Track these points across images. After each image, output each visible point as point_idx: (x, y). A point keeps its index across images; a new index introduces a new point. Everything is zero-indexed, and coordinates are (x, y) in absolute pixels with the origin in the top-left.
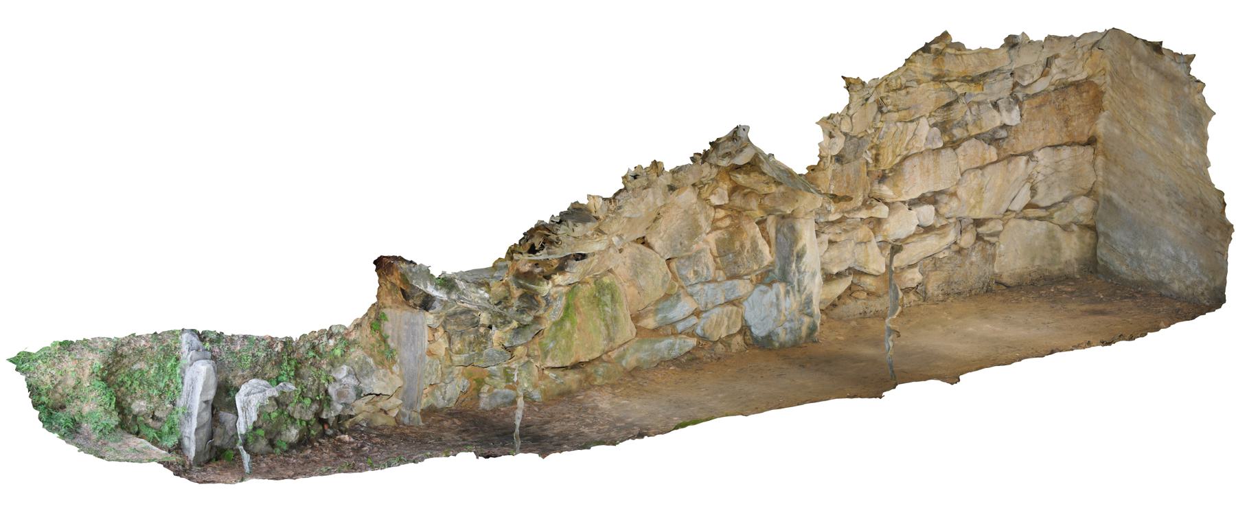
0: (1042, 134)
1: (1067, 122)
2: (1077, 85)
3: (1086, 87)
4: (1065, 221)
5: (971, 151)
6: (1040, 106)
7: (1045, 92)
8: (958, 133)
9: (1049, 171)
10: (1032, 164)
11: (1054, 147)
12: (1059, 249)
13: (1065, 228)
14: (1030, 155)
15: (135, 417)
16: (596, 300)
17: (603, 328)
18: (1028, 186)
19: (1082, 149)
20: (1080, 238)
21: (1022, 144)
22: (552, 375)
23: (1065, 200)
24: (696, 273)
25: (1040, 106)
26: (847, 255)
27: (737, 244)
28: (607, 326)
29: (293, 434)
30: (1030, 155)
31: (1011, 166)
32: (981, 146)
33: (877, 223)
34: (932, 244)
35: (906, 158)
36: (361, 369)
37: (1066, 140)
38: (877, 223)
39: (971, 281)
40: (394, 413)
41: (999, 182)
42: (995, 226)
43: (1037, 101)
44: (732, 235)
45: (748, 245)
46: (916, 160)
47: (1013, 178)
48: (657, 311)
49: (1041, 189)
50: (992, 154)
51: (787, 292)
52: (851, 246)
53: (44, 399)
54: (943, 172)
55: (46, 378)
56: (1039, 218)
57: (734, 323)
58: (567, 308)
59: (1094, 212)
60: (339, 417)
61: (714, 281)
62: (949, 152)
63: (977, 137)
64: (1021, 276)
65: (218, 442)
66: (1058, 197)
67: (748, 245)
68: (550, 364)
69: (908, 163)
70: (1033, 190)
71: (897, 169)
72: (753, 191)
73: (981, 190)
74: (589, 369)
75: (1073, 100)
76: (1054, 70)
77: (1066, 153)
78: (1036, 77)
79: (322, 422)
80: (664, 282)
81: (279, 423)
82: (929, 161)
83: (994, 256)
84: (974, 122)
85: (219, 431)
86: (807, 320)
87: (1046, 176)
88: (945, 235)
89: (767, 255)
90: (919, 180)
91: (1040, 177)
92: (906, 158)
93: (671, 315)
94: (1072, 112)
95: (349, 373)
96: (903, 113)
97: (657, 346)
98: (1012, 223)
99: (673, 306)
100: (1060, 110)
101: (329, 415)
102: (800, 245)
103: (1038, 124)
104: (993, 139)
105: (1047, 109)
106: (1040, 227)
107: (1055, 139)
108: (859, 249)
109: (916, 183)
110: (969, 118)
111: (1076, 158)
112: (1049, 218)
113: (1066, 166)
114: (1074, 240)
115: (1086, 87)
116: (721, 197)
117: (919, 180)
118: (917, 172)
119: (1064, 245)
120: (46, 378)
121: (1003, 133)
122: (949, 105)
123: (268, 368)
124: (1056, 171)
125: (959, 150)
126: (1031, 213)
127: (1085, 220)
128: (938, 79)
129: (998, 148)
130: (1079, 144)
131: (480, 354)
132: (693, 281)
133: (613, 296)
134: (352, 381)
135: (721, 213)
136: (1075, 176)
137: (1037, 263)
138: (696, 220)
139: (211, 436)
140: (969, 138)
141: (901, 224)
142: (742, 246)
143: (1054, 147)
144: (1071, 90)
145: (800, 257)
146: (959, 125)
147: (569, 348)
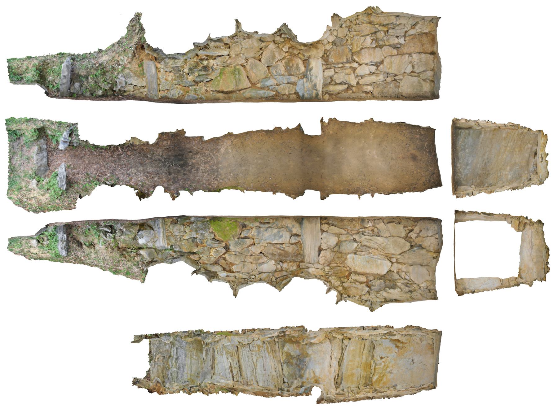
0: (413, 48)
1: (423, 45)
2: (426, 34)
3: (429, 35)
4: (425, 78)
5: (386, 50)
6: (413, 39)
7: (414, 35)
8: (381, 43)
9: (418, 61)
10: (410, 58)
11: (419, 53)
12: (422, 87)
13: (424, 80)
14: (410, 54)
15: (49, 82)
16: (233, 73)
17: (234, 82)
18: (410, 65)
19: (429, 55)
20: (430, 84)
21: (406, 50)
22: (211, 92)
23: (424, 71)
24: (276, 71)
25: (413, 39)
26: (341, 77)
27: (291, 64)
28: (236, 81)
29: (100, 92)
30: (410, 54)
31: (403, 57)
32: (390, 48)
33: (354, 70)
34: (373, 78)
35: (362, 49)
36: (127, 75)
37: (422, 51)
38: (354, 70)
39: (390, 93)
40: (145, 93)
41: (398, 61)
42: (400, 77)
43: (411, 37)
44: (289, 61)
45: (295, 65)
46: (366, 50)
47: (404, 61)
48: (261, 82)
49: (416, 67)
50: (395, 52)
51: (307, 81)
52: (343, 74)
53: (14, 71)
54: (378, 55)
55: (16, 65)
56: (415, 76)
57: (291, 90)
58: (220, 73)
59: (433, 76)
60: (120, 90)
61: (283, 75)
62: (379, 49)
63: (390, 45)
64: (410, 94)
65: (72, 91)
66: (421, 70)
67: (295, 65)
68: (211, 89)
69: (363, 50)
70: (413, 67)
71: (359, 52)
72: (296, 48)
73: (391, 63)
74: (230, 95)
75: (425, 38)
76: (417, 27)
77: (423, 55)
78: (409, 29)
79: (114, 91)
80: (265, 73)
81: (95, 88)
82: (371, 51)
83: (399, 87)
84: (387, 40)
85: (72, 88)
86: (315, 91)
87: (417, 63)
88: (378, 76)
89: (303, 69)
90: (367, 56)
91: (415, 63)
92: (362, 49)
93: (266, 83)
94: (424, 42)
95: (122, 76)
96: (358, 33)
97: (258, 92)
98: (406, 77)
99: (267, 81)
100: (420, 41)
101: (116, 89)
102: (311, 66)
103: (412, 44)
104: (395, 47)
105: (415, 40)
106: (416, 79)
107: (418, 50)
108: (346, 76)
109: (366, 57)
110: (385, 38)
111: (427, 58)
112: (419, 76)
113: (423, 60)
114: (428, 85)
115: (429, 35)
116: (286, 49)
117: (367, 56)
118: (367, 54)
119: (424, 86)
120: (16, 65)
121: (399, 46)
122: (375, 32)
123: (92, 70)
124: (420, 61)
125: (383, 49)
126: (413, 74)
127: (431, 79)
128: (370, 23)
129: (398, 50)
130: (428, 53)
131: (182, 81)
132: (275, 74)
133: (239, 73)
134: (123, 79)
135: (287, 54)
136: (426, 64)
137: (415, 91)
138: (274, 54)
139: (70, 89)
140: (385, 45)
141: (363, 70)
142: (293, 65)
143: (419, 53)
144: (424, 35)
145: (311, 70)
146: (381, 40)
147: (218, 85)
